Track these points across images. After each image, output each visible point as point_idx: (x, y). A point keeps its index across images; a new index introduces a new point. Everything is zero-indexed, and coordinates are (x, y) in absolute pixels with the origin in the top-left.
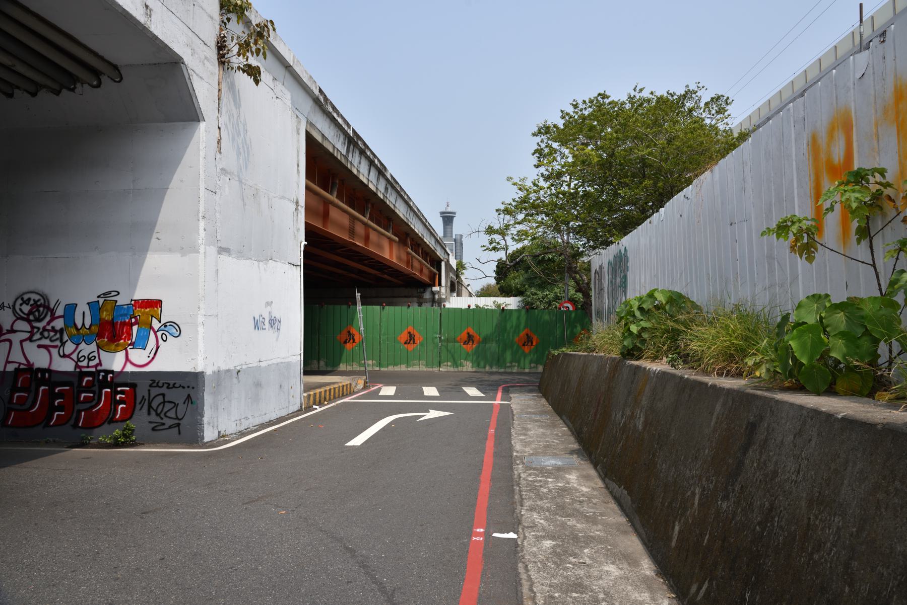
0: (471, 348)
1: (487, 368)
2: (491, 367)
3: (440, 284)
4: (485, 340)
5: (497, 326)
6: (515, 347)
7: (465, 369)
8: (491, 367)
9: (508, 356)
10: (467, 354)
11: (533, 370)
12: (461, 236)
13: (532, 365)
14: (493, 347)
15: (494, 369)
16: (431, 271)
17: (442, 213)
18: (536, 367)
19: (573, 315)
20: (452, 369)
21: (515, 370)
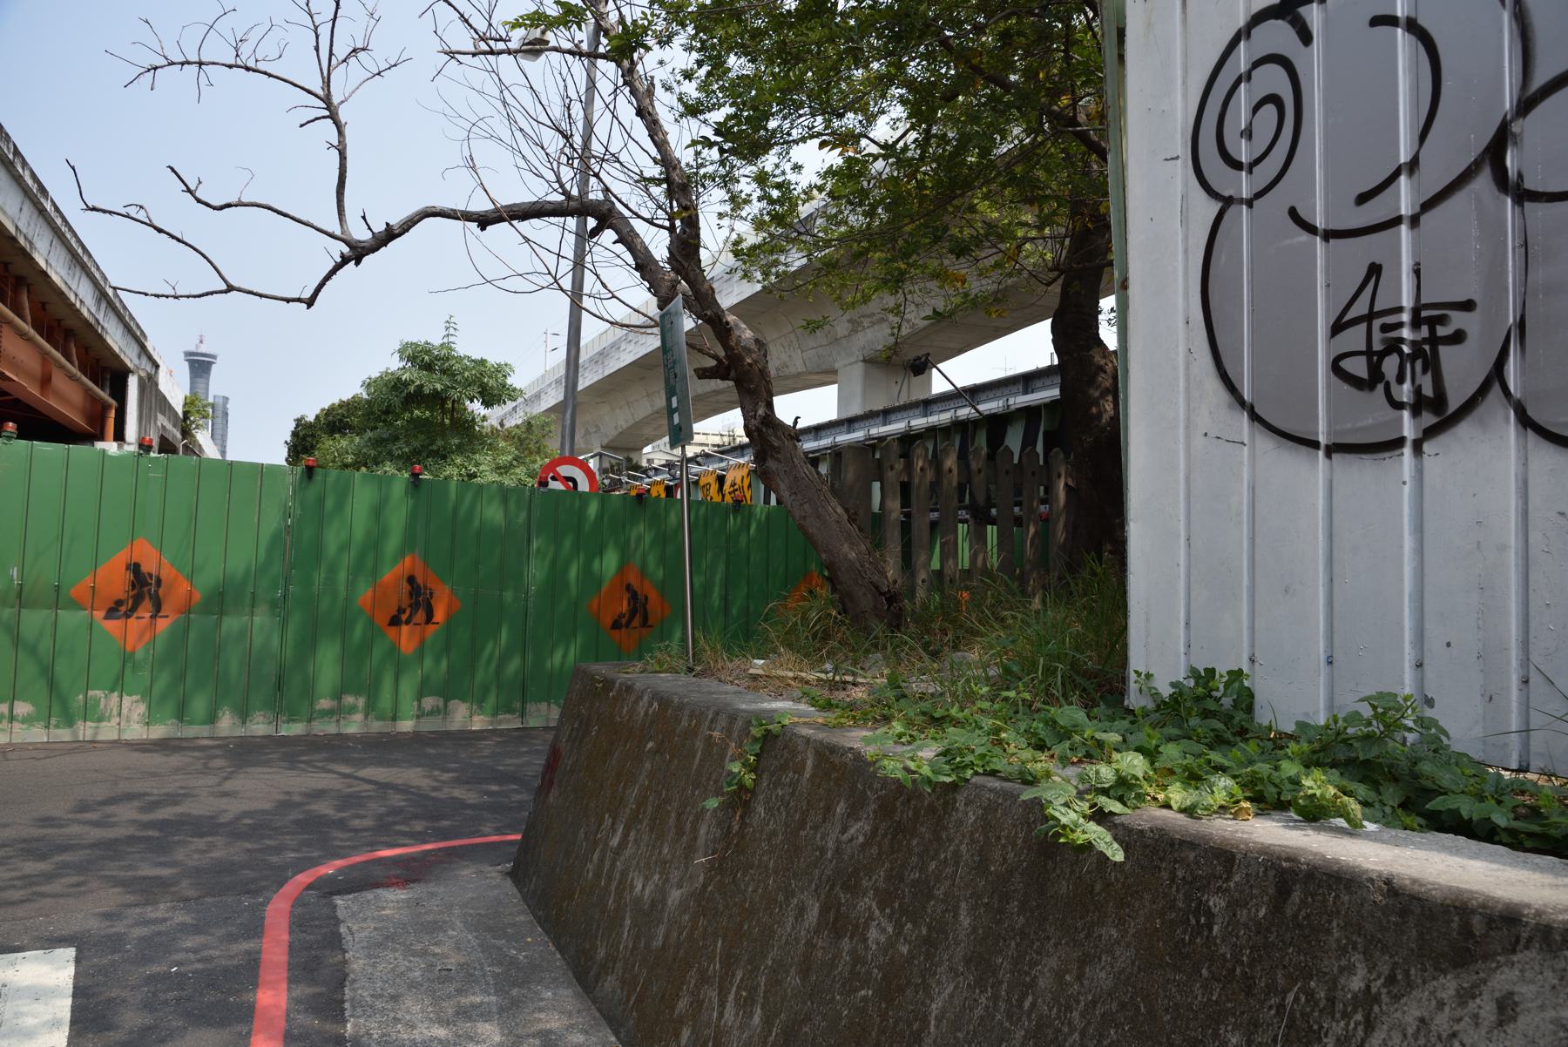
0: (142, 633)
1: (227, 724)
2: (244, 715)
3: (120, 436)
4: (220, 600)
5: (276, 539)
6: (358, 632)
7: (108, 732)
8: (244, 715)
9: (327, 665)
10: (127, 658)
11: (430, 725)
12: (226, 399)
13: (429, 702)
14: (258, 626)
15: (259, 727)
16: (93, 399)
17: (188, 354)
18: (444, 712)
19: (593, 509)
20: (38, 734)
21: (354, 726)
